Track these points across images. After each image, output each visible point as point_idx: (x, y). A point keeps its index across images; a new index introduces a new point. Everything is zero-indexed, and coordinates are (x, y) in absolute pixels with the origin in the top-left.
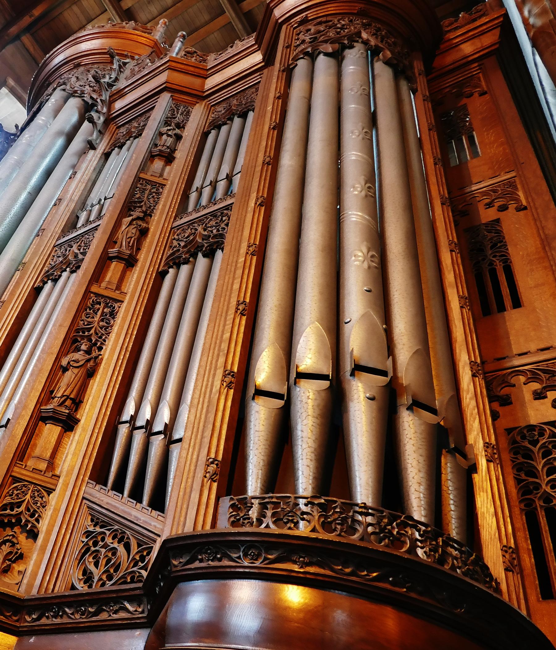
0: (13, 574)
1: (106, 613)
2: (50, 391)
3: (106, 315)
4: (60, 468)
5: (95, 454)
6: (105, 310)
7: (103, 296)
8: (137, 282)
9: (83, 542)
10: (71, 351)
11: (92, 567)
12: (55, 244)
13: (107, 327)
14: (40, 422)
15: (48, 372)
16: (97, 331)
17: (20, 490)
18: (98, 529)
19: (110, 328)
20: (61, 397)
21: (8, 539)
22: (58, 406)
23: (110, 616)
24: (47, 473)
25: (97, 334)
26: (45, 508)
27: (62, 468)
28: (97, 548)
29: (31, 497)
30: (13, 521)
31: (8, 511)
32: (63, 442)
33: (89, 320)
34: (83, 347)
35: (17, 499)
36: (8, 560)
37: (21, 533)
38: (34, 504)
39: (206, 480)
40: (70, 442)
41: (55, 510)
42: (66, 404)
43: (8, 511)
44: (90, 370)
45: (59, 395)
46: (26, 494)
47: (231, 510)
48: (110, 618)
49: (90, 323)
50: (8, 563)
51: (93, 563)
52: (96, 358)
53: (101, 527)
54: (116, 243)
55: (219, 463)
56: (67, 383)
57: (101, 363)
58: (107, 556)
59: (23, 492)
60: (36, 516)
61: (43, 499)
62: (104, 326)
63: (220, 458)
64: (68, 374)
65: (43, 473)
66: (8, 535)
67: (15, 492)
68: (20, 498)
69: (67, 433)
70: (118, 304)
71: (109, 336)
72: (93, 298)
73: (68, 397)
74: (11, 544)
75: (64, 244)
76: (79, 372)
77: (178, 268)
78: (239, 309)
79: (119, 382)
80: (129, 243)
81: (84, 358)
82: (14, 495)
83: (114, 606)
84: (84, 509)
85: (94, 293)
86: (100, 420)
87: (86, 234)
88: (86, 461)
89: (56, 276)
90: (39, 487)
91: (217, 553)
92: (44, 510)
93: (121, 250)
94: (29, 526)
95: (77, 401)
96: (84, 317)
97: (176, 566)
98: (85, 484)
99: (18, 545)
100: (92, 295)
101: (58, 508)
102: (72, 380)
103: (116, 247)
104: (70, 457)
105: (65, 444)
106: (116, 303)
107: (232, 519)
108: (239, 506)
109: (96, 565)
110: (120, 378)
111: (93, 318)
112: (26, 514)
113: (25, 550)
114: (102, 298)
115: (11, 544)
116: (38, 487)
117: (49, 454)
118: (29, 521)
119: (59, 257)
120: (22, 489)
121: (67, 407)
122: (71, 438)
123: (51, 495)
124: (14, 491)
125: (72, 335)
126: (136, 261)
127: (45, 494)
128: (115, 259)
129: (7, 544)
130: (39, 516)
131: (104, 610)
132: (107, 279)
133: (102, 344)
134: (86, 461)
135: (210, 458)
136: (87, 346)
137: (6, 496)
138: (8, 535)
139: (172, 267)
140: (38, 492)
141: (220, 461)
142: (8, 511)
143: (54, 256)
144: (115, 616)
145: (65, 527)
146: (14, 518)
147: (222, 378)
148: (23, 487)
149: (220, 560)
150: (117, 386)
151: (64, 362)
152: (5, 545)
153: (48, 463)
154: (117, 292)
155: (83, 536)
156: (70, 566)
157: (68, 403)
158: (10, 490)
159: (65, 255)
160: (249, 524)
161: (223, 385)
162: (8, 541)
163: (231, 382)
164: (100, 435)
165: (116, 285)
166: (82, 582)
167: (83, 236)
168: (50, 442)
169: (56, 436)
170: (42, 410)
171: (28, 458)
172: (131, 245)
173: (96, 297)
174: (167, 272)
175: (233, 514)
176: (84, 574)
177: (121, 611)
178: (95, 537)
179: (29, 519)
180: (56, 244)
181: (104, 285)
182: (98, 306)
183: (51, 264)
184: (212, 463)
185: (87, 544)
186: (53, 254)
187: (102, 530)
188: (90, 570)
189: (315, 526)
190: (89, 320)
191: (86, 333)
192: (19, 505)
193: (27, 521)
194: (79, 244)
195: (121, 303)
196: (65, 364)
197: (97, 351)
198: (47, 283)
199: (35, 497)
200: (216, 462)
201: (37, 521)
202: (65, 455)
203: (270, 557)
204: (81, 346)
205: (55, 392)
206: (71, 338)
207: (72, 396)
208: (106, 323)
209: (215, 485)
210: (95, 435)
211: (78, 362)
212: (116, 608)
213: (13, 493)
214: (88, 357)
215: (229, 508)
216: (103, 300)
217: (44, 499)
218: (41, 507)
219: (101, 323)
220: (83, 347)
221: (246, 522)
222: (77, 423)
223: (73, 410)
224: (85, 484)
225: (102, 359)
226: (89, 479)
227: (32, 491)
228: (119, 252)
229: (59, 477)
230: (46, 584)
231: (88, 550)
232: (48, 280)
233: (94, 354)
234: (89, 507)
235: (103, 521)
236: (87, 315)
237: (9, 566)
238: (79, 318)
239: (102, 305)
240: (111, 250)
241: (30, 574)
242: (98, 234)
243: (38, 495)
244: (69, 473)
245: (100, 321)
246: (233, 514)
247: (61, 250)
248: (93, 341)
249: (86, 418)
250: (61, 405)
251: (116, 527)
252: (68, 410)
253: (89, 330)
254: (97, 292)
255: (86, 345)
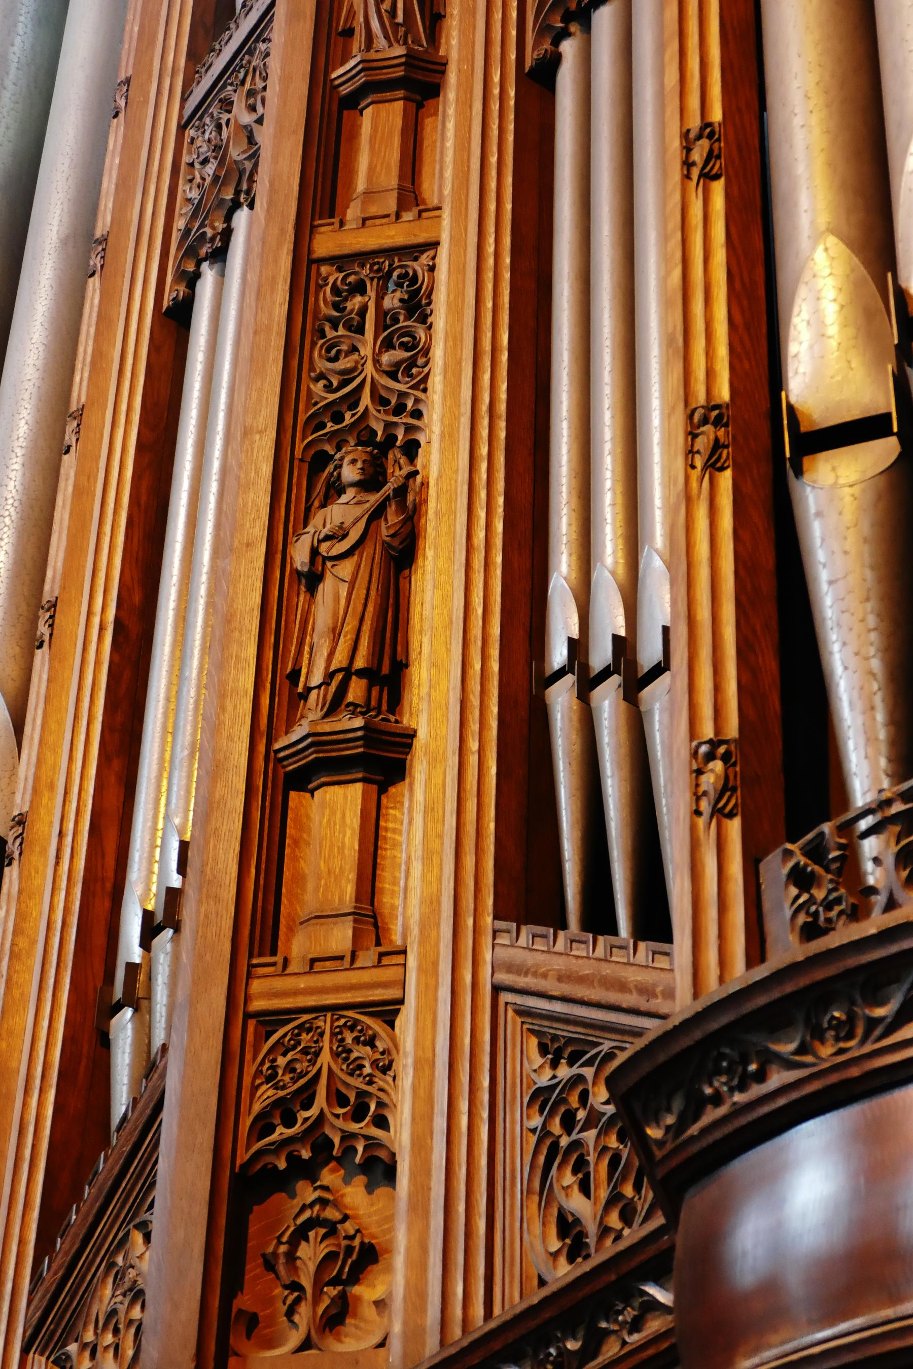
0: (365, 1321)
1: (613, 1338)
2: (289, 677)
3: (396, 320)
4: (400, 918)
5: (492, 826)
6: (387, 303)
7: (362, 257)
8: (463, 145)
9: (533, 1131)
10: (316, 504)
11: (577, 1204)
12: (181, 116)
13: (412, 363)
14: (293, 794)
15: (257, 613)
16: (383, 393)
17: (294, 1048)
18: (564, 1072)
19: (421, 361)
20: (326, 683)
21: (310, 1219)
22: (324, 717)
23: (624, 1343)
24: (360, 954)
25: (384, 402)
26: (391, 1073)
27: (404, 917)
28: (574, 1136)
29: (335, 1055)
30: (306, 1154)
31: (281, 1132)
32: (386, 829)
33: (344, 363)
34: (350, 473)
35: (294, 1080)
36: (328, 1284)
37: (347, 1181)
38: (351, 1074)
39: (701, 822)
40: (406, 821)
41: (418, 1065)
42: (350, 698)
43: (280, 1130)
44: (396, 543)
45: (317, 678)
46: (317, 1054)
47: (794, 891)
48: (627, 1349)
49: (347, 376)
50: (332, 1291)
51: (576, 1188)
52: (401, 491)
53: (571, 1064)
54: (349, 33)
55: (733, 748)
56: (330, 622)
57: (426, 501)
58: (605, 1149)
59: (305, 1051)
60: (373, 1107)
61: (378, 1043)
62: (398, 364)
63: (732, 729)
64: (327, 587)
65: (347, 962)
66: (304, 1208)
67: (282, 1061)
68: (302, 1075)
69: (392, 790)
70: (425, 259)
71: (425, 390)
72: (331, 280)
73: (348, 672)
74: (322, 1231)
75: (209, 106)
76: (358, 566)
77: (587, 27)
78: (694, 164)
79: (498, 542)
80: (393, 13)
81: (358, 511)
82: (280, 1072)
83: (624, 1309)
84: (512, 1023)
85: (330, 260)
86: (475, 700)
87: (257, 41)
88: (469, 861)
89: (213, 239)
90: (350, 1013)
91: (746, 1062)
92: (390, 1080)
93: (372, 55)
94: (360, 1149)
95: (386, 669)
96: (322, 365)
97: (661, 1143)
98: (487, 940)
99: (347, 1224)
100: (324, 269)
101: (429, 1054)
102: (343, 602)
103: (355, 50)
104: (417, 869)
105: (395, 831)
106: (416, 259)
107: (802, 919)
108: (809, 869)
109: (585, 1188)
110: (499, 526)
111: (354, 349)
112: (337, 1116)
113: (374, 1231)
114: (363, 266)
115: (322, 1231)
116: (345, 1013)
117: (349, 890)
118: (353, 1136)
119: (205, 162)
120: (299, 1043)
121: (356, 706)
122: (406, 804)
123: (398, 1023)
124: (274, 1060)
125: (300, 447)
126: (441, 67)
127: (376, 1025)
128: (365, 96)
129: (312, 1234)
130: (381, 1104)
131: (607, 1333)
132: (361, 184)
133: (410, 429)
134: (469, 861)
135: (700, 744)
136: (359, 465)
137: (255, 1088)
138: (304, 1208)
139: (565, 34)
140: (352, 1029)
141: (735, 741)
142: (281, 1132)
143: (192, 165)
144: (634, 1338)
145: (463, 1106)
146: (304, 1147)
147: (686, 440)
148: (299, 1035)
149: (760, 1076)
150: (499, 559)
151: (300, 556)
152: (307, 1240)
153: (355, 921)
154: (408, 216)
155: (531, 1111)
156: (518, 1224)
157: (356, 691)
158: (262, 1063)
159: (220, 148)
160: (844, 917)
161: (693, 467)
162: (311, 1224)
163: (717, 445)
164: (488, 753)
165: (395, 194)
166: (562, 1260)
167: (251, 52)
168: (341, 849)
169: (353, 820)
170: (282, 754)
171: (291, 930)
172: (400, 19)
173: (339, 269)
174: (555, 60)
175: (801, 900)
176: (563, 1232)
177: (649, 1316)
178: (561, 1101)
179: (354, 1127)
180: (186, 116)
181: (353, 213)
182: (358, 300)
183: (189, 200)
184: (710, 757)
185: (544, 1133)
186: (186, 159)
187: (575, 1070)
188: (573, 1214)
189: (322, 1110)
190: (344, 363)
191: (348, 418)
192: (306, 1097)
193: (348, 1137)
194: (247, 86)
195: (431, 253)
196: (303, 563)
197: (403, 461)
198: (197, 275)
199: (350, 1051)
200: (722, 750)
201: (381, 1122)
202: (403, 867)
203: (880, 1012)
204: (339, 475)
205: (304, 671)
206: (301, 460)
207: (360, 663)
208: (405, 347)
209: (734, 827)
210: (473, 760)
211: (345, 536)
212: (629, 1314)
213: (274, 1068)
214: (374, 499)
215: (786, 886)
216: (366, 271)
217: (380, 1045)
218: (378, 1073)
219: (386, 358)
220: (350, 473)
221: (833, 914)
222: (410, 746)
223: (384, 707)
224: (487, 940)
225: (425, 485)
226: (496, 918)
227: (333, 1035)
228: (367, 66)
229: (404, 952)
230: (459, 1312)
231: (554, 1148)
232: (198, 264)
233: (395, 476)
234: (522, 1012)
235: (570, 1041)
236: (328, 350)
237: (343, 1296)
238: (304, 375)
239: (371, 292)
240: (341, 71)
241: (405, 1299)
242: (278, 32)
243: (356, 1040)
244: (429, 923)
245: (380, 353)
246: (801, 900)
247: (203, 133)
248: (380, 433)
249: (430, 714)
250: (333, 708)
251: (606, 1046)
252: (363, 714)
253: (353, 400)
254: (337, 252)
255: (354, 462)
